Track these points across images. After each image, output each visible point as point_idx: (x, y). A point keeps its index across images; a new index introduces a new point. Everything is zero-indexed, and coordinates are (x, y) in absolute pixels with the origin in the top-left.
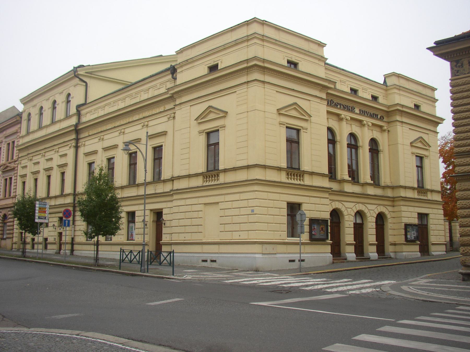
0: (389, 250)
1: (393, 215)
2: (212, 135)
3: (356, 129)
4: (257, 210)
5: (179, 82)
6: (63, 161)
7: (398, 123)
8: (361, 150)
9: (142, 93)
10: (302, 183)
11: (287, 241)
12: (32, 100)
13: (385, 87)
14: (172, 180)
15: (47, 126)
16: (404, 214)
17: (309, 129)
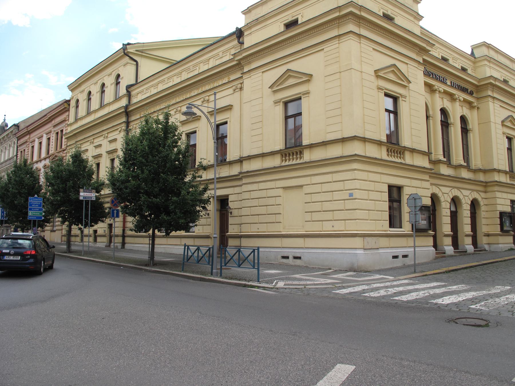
0: (483, 241)
1: (486, 202)
2: (290, 105)
3: (447, 104)
4: (357, 194)
5: (246, 46)
6: (112, 147)
7: (490, 99)
8: (452, 128)
9: (202, 64)
10: (403, 161)
11: (389, 232)
12: (80, 85)
13: (473, 58)
14: (241, 161)
15: (95, 111)
16: (499, 201)
17: (408, 98)
